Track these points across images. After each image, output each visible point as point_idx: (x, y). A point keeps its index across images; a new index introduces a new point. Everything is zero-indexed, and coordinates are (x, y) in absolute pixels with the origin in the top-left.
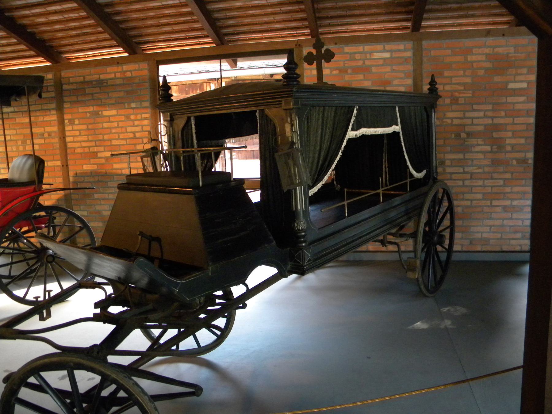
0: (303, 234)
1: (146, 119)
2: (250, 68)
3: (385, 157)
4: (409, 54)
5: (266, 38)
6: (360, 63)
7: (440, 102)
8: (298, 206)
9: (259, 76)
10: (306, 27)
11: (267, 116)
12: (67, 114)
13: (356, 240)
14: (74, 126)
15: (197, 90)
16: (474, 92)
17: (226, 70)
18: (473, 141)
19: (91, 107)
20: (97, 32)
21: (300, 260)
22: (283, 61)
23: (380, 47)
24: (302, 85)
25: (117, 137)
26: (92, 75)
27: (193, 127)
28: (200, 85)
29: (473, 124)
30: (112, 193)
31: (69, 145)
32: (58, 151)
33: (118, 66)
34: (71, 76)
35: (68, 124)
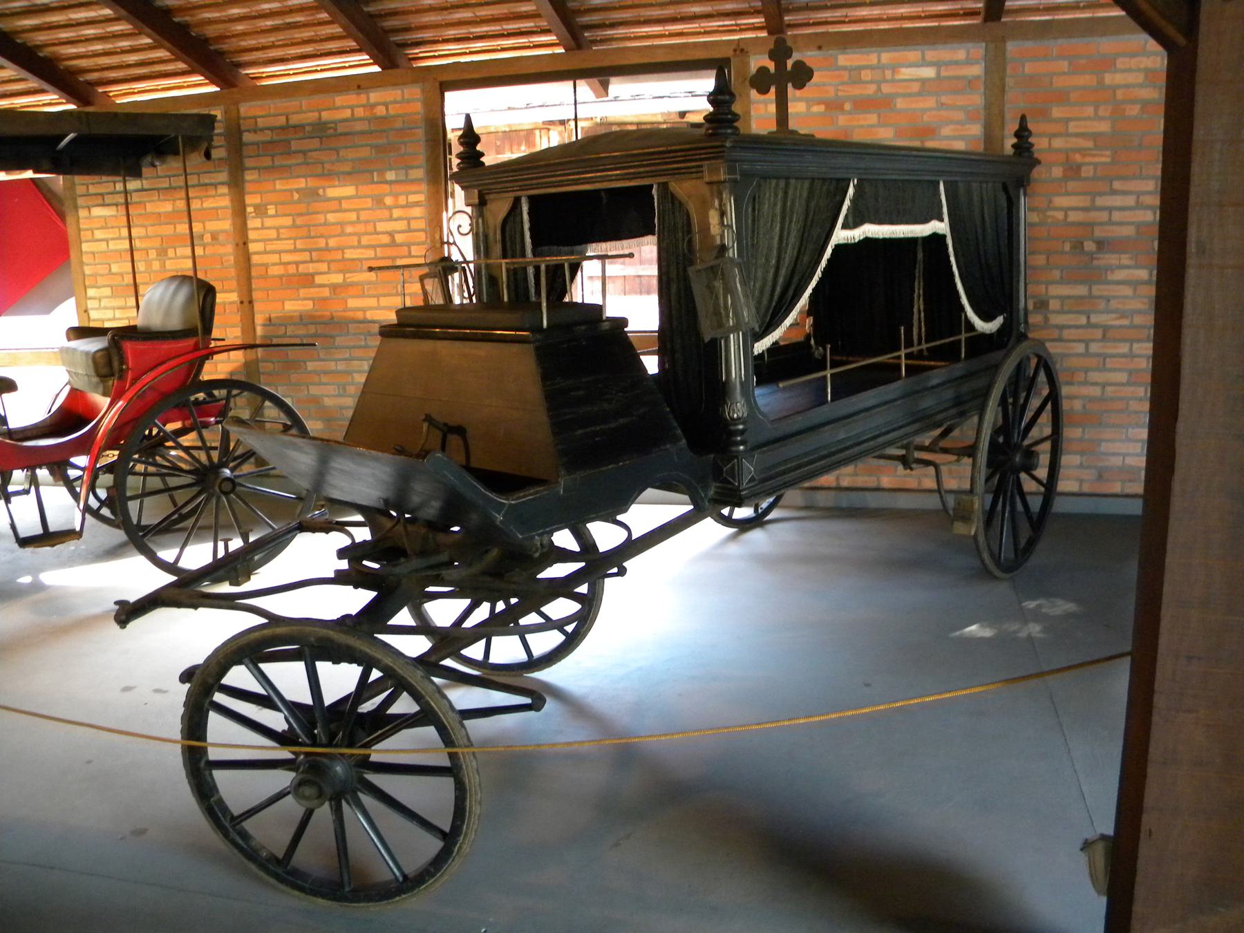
0: (741, 427)
1: (417, 204)
2: (636, 97)
3: (919, 289)
4: (977, 70)
5: (672, 35)
6: (871, 90)
7: (1037, 172)
8: (731, 373)
9: (655, 115)
10: (756, 12)
11: (673, 195)
12: (253, 193)
13: (847, 448)
14: (265, 219)
15: (519, 145)
16: (1116, 152)
17: (584, 103)
18: (1110, 259)
19: (303, 180)
20: (316, 22)
21: (734, 478)
22: (707, 83)
23: (913, 54)
24: (743, 135)
25: (356, 243)
26: (305, 112)
27: (526, 217)
28: (529, 135)
29: (1110, 222)
30: (344, 360)
31: (255, 259)
32: (232, 272)
33: (358, 94)
34: (261, 114)
35: (254, 214)
